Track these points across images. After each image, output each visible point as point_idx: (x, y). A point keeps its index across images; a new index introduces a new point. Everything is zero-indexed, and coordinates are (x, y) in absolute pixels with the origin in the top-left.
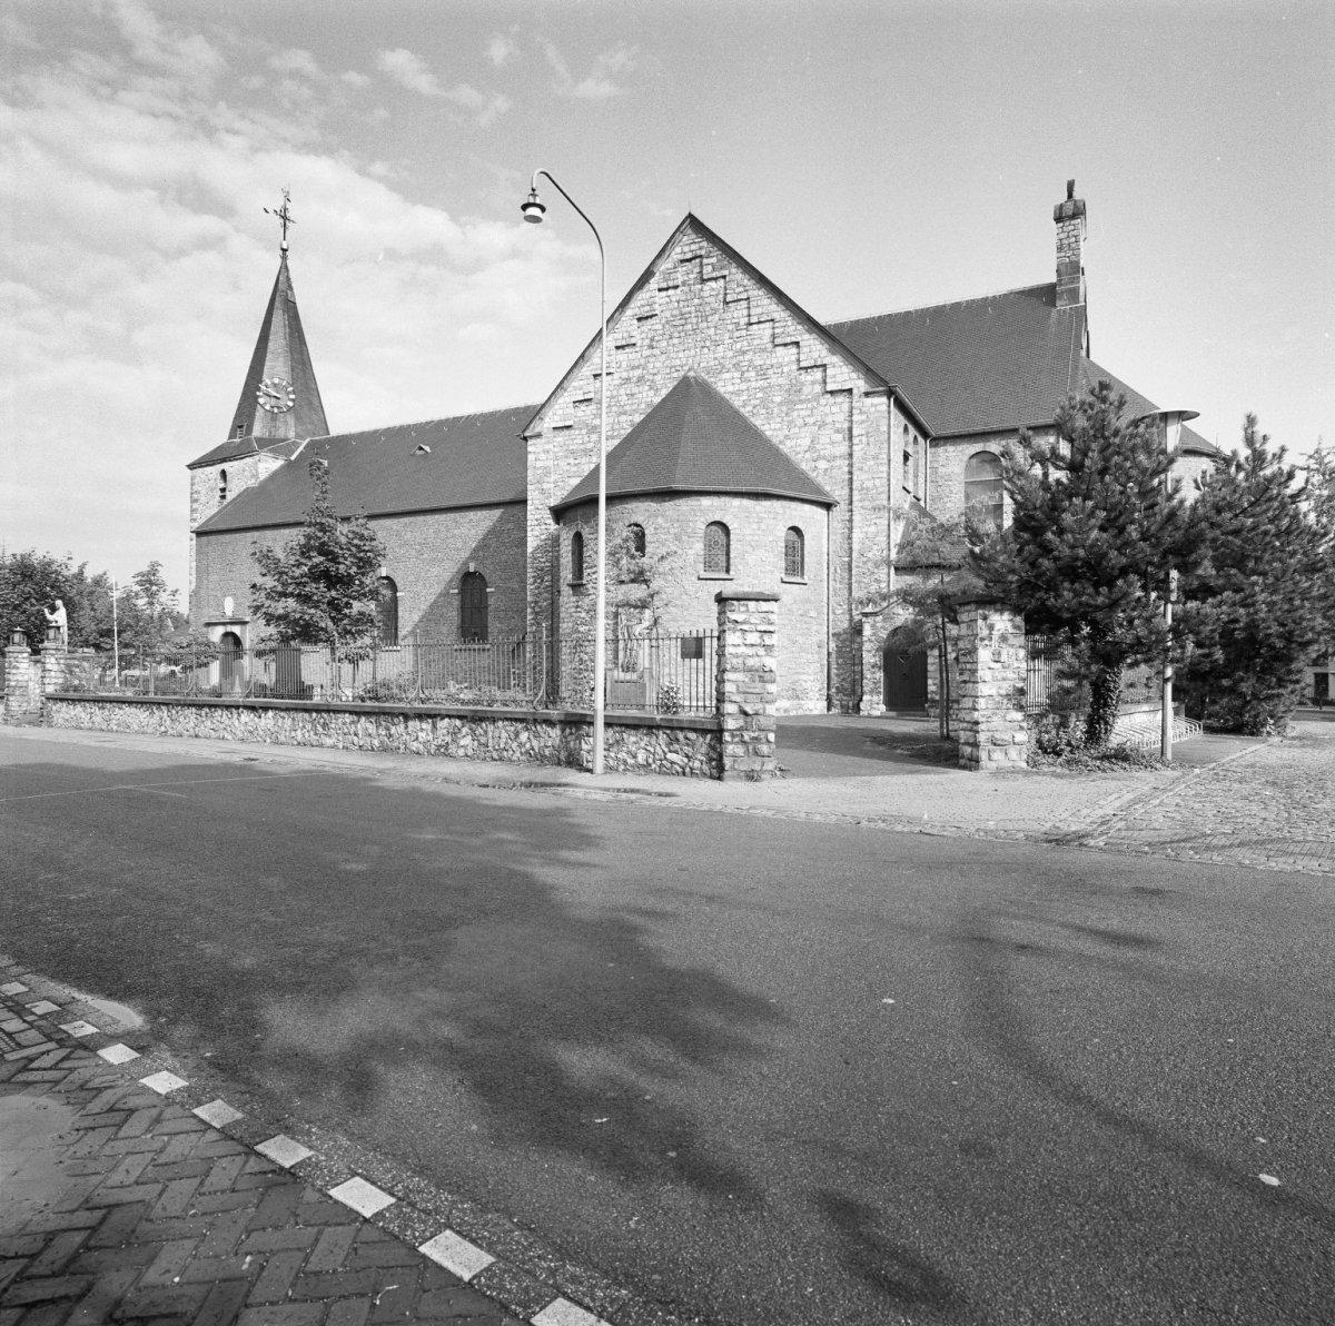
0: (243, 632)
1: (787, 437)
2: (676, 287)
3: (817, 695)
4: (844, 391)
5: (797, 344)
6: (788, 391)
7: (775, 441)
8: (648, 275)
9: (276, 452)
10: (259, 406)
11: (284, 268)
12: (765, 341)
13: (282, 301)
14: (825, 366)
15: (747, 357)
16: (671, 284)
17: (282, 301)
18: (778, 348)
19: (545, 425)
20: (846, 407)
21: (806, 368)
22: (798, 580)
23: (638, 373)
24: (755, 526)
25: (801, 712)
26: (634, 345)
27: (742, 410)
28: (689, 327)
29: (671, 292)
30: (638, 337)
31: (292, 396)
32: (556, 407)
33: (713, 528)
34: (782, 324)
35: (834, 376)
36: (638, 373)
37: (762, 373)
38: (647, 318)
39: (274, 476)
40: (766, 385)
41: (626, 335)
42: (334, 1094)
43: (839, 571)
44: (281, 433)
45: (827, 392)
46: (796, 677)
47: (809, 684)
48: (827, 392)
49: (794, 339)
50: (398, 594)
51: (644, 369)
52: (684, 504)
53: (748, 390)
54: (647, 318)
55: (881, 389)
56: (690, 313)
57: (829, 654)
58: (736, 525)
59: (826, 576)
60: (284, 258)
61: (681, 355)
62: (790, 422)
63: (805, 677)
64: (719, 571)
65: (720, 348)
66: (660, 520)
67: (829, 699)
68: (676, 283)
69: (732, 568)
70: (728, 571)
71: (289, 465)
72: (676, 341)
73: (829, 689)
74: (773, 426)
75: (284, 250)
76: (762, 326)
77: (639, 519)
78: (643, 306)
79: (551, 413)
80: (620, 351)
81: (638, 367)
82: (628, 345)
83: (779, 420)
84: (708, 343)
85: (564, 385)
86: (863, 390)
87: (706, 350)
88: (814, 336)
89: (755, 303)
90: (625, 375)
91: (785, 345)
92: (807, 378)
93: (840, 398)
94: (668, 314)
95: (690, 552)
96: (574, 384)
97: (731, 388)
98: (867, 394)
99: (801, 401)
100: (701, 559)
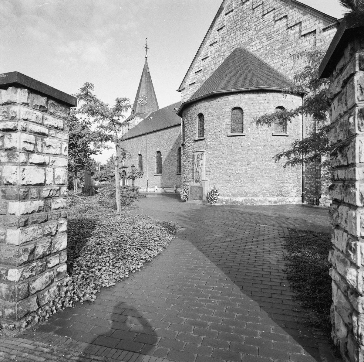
0: (126, 170)
1: (281, 65)
2: (232, 10)
3: (295, 194)
4: (310, 33)
5: (286, 17)
6: (282, 42)
7: (276, 68)
8: (221, 9)
9: (141, 117)
10: (138, 104)
11: (146, 63)
12: (271, 21)
13: (146, 74)
14: (300, 23)
15: (263, 32)
16: (230, 10)
17: (146, 74)
18: (277, 22)
19: (187, 84)
20: (312, 41)
21: (291, 27)
22: (284, 134)
23: (218, 54)
24: (257, 107)
25: (284, 203)
26: (216, 42)
27: (261, 57)
28: (238, 26)
29: (231, 14)
30: (218, 38)
31: (147, 100)
32: (190, 76)
33: (235, 111)
34: (279, 9)
35: (306, 26)
36: (218, 54)
37: (269, 37)
38: (221, 29)
39: (140, 124)
40: (271, 42)
41: (213, 39)
42: (272, 258)
43: (309, 129)
44: (143, 111)
45: (302, 36)
46: (281, 185)
47: (290, 188)
48: (302, 36)
49: (285, 14)
50: (162, 156)
51: (220, 51)
52: (220, 101)
53: (263, 47)
54: (221, 29)
55: (332, 24)
56: (238, 20)
57: (303, 172)
58: (246, 108)
59: (301, 132)
60: (146, 60)
61: (234, 40)
62: (283, 57)
63: (287, 185)
64: (238, 132)
65: (251, 32)
66: (210, 110)
67: (303, 197)
68: (232, 9)
69: (244, 130)
70: (242, 132)
71: (145, 120)
72: (232, 35)
73: (303, 191)
74: (275, 62)
75: (146, 58)
76: (269, 14)
77: (201, 111)
78: (219, 24)
79: (188, 79)
80: (212, 46)
81: (218, 51)
82: (214, 43)
83: (277, 57)
84: (245, 31)
85: (192, 67)
86: (322, 28)
87: (244, 34)
88: (295, 9)
89: (266, 4)
90: (213, 56)
91: (280, 19)
92: (291, 32)
93: (309, 37)
94: (229, 24)
95: (223, 123)
96: (196, 65)
97: (255, 49)
98: (324, 30)
99: (289, 45)
100: (230, 126)
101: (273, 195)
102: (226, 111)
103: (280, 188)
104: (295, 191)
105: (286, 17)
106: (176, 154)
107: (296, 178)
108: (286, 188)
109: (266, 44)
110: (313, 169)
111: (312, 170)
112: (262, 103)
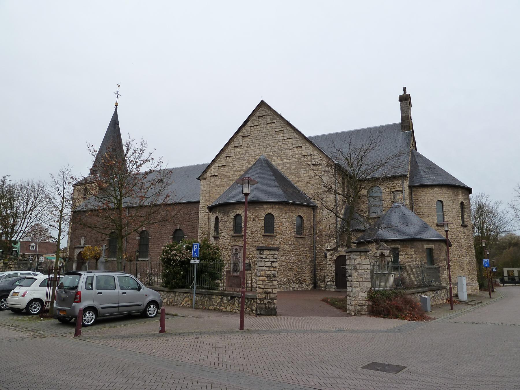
27: (333, 270)
76: (288, 140)
96: (219, 160)
100: (263, 228)
101: (295, 283)
102: (261, 216)
103: (300, 277)
104: (310, 279)
105: (301, 147)
106: (170, 237)
107: (310, 270)
108: (304, 277)
109: (285, 161)
110: (321, 263)
111: (320, 264)
112: (288, 212)
